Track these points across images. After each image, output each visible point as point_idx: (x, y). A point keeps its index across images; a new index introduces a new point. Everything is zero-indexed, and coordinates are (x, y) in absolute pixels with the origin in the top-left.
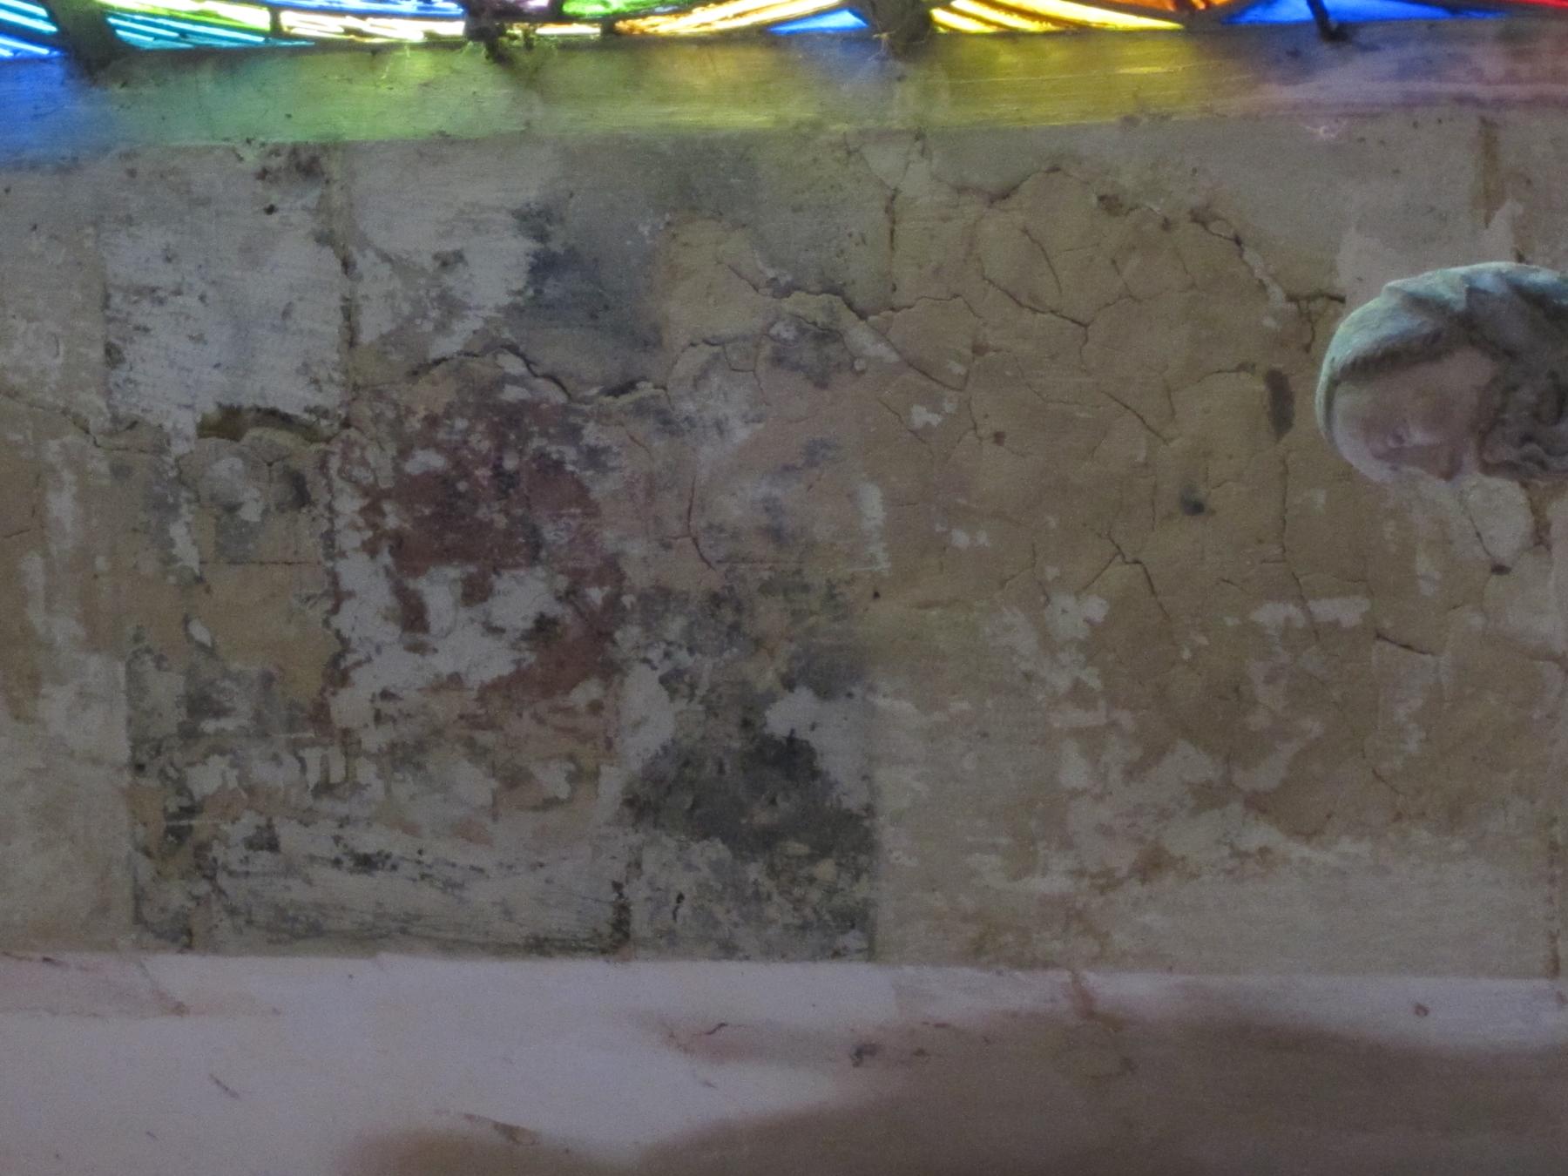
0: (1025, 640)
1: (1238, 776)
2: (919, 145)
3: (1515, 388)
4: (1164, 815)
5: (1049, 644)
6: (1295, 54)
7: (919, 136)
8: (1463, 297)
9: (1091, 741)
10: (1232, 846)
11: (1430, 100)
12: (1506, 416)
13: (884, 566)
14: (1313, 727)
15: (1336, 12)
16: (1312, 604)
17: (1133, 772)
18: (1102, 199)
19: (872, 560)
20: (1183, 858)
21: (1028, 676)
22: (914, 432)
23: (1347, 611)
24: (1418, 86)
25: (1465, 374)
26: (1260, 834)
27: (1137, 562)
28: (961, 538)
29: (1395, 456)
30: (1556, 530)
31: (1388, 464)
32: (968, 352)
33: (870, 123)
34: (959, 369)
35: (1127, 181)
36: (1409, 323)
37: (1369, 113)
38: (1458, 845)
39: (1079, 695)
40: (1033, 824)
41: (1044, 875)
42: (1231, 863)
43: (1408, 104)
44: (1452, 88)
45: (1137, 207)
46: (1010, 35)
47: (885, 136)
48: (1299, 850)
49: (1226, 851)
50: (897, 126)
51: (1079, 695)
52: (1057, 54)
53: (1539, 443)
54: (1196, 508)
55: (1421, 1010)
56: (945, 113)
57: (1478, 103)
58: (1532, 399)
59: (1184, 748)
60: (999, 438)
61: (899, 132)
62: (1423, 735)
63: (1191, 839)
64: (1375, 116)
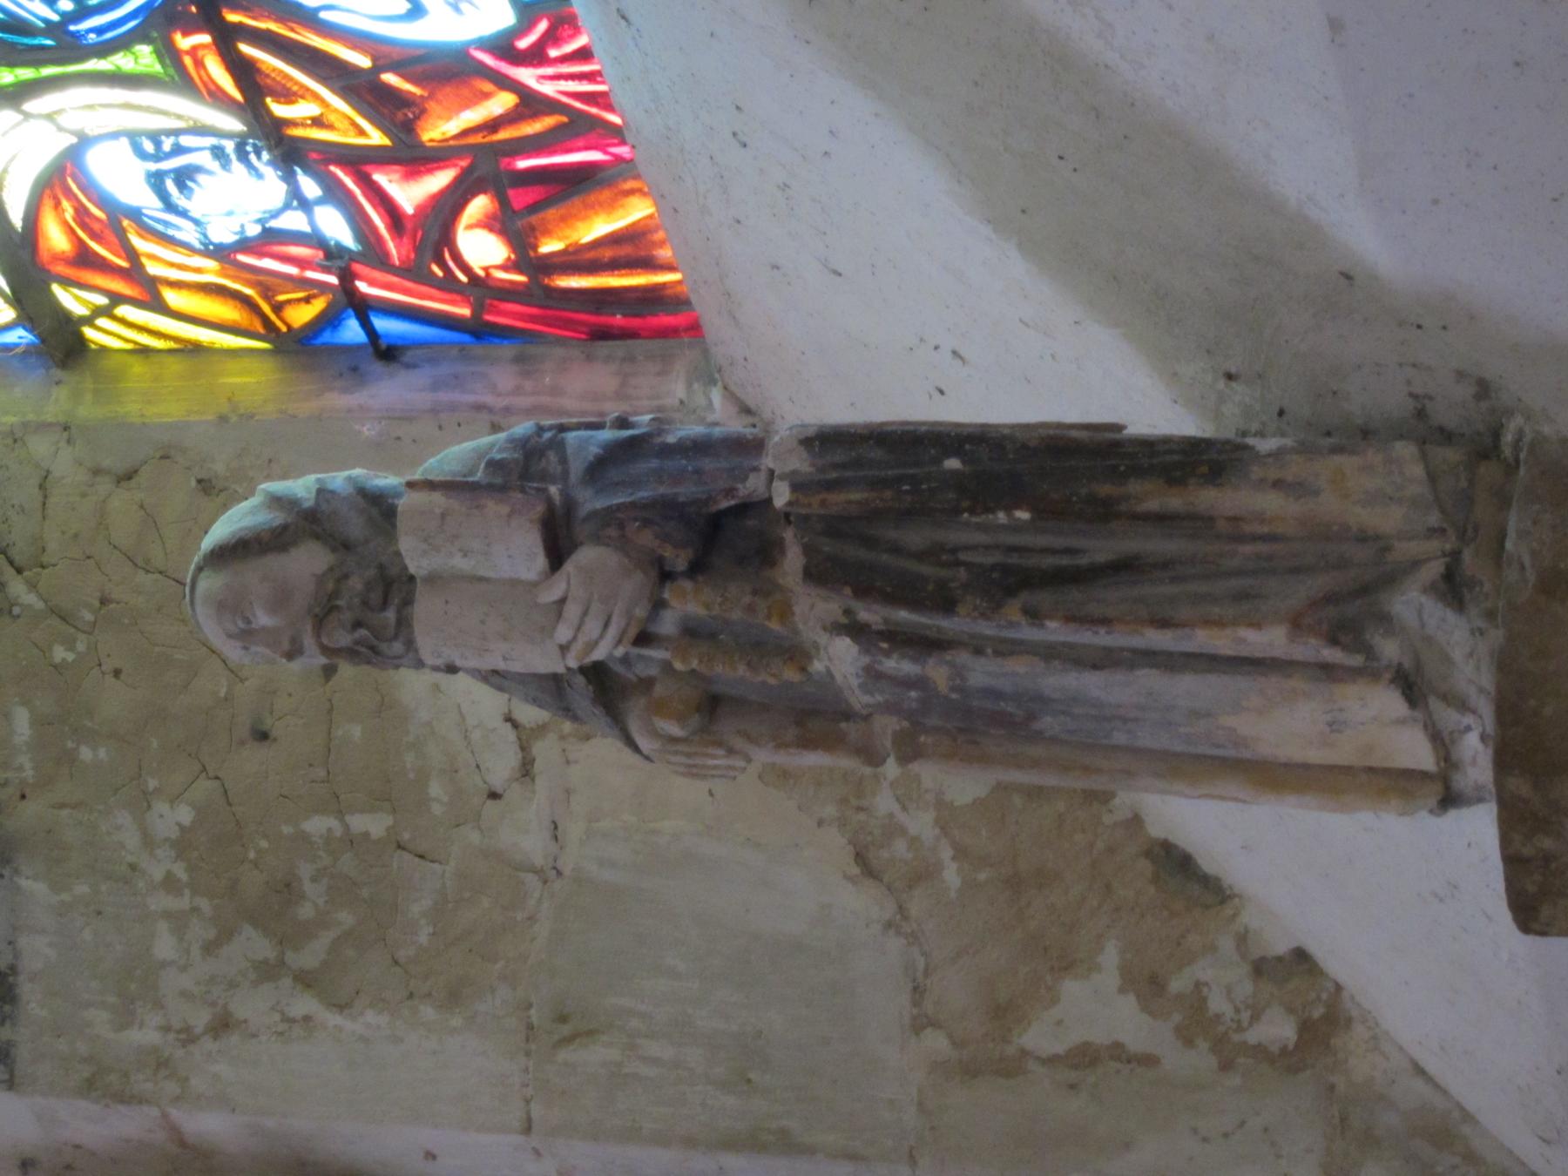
0: (131, 839)
1: (290, 957)
2: (65, 435)
3: (346, 576)
4: (233, 985)
5: (148, 842)
6: (355, 369)
7: (66, 428)
8: (313, 495)
9: (179, 922)
10: (283, 1013)
11: (453, 408)
12: (339, 603)
13: (29, 773)
14: (346, 918)
15: (387, 336)
16: (347, 818)
17: (209, 949)
18: (199, 481)
19: (21, 768)
20: (245, 1021)
21: (133, 867)
22: (55, 667)
23: (374, 824)
24: (445, 396)
25: (307, 563)
26: (304, 1004)
27: (217, 778)
28: (86, 753)
29: (247, 635)
30: (538, 766)
31: (239, 644)
32: (97, 603)
33: (31, 417)
34: (89, 617)
35: (219, 468)
36: (275, 518)
37: (408, 417)
38: (456, 1022)
39: (170, 884)
40: (133, 986)
41: (140, 1028)
42: (281, 1028)
43: (435, 411)
44: (470, 398)
45: (225, 489)
46: (144, 351)
47: (43, 427)
48: (334, 1019)
49: (277, 1017)
50: (50, 419)
51: (170, 884)
52: (175, 366)
53: (368, 628)
54: (263, 736)
55: (430, 1156)
56: (88, 411)
57: (490, 410)
58: (359, 587)
59: (248, 931)
60: (117, 673)
61: (50, 425)
62: (431, 930)
63: (252, 1005)
64: (410, 419)
